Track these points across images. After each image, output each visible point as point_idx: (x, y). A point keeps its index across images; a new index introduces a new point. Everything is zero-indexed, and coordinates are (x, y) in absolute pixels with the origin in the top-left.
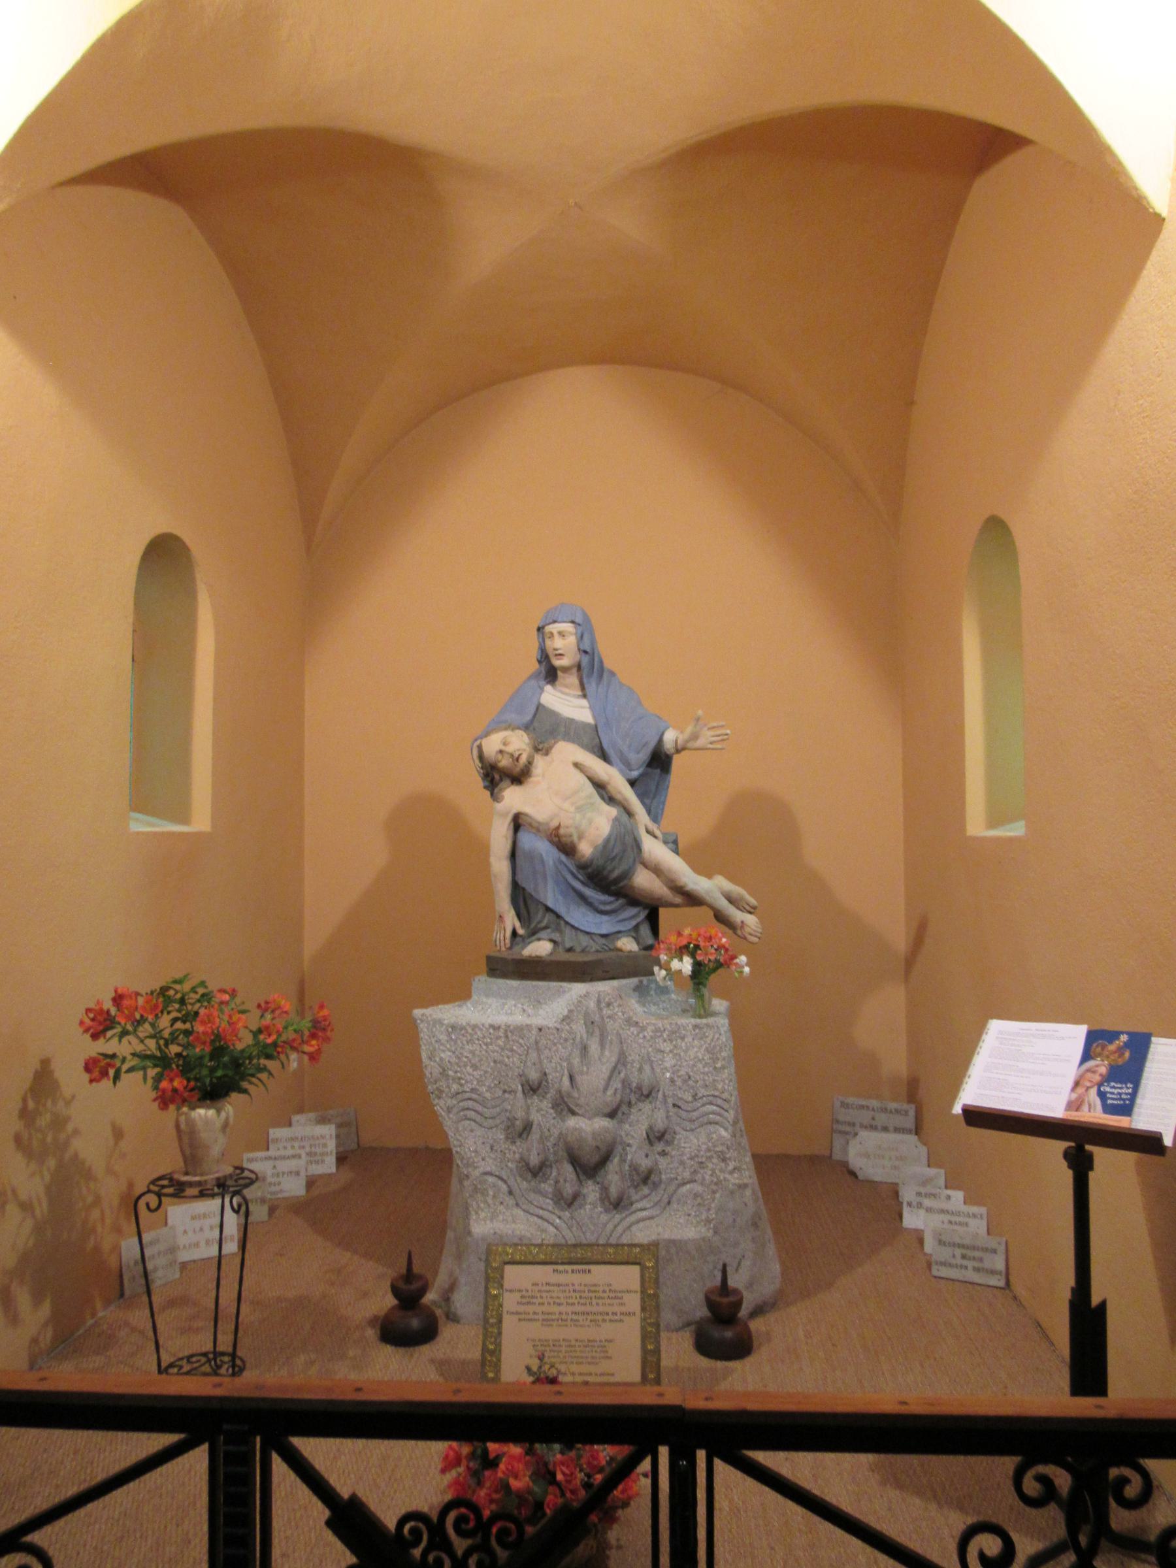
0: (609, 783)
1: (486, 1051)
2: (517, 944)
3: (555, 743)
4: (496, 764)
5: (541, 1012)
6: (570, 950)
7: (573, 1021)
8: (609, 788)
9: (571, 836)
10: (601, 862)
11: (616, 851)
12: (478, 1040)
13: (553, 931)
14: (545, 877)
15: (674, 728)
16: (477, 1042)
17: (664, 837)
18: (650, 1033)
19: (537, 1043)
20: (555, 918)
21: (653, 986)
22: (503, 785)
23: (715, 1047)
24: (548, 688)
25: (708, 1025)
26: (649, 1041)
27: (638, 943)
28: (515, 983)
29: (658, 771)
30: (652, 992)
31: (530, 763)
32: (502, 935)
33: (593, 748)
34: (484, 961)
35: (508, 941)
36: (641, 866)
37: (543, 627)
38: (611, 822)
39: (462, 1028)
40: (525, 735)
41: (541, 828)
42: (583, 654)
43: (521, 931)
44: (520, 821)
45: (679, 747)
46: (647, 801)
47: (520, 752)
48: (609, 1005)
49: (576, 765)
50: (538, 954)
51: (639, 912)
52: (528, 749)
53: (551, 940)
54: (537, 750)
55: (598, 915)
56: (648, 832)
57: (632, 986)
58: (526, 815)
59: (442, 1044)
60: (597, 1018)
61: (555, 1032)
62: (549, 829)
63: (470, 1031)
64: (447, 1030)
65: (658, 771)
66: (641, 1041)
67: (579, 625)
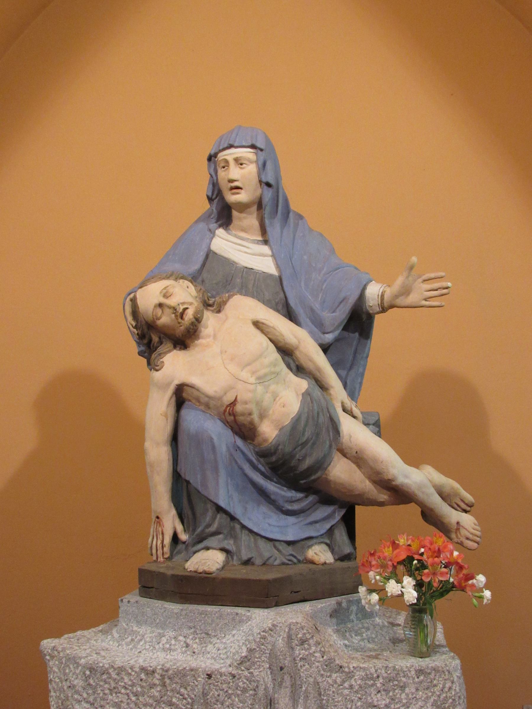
0: (297, 348)
1: (136, 704)
2: (179, 552)
3: (230, 297)
4: (154, 322)
5: (210, 647)
6: (248, 562)
7: (254, 663)
8: (297, 353)
9: (250, 414)
10: (288, 449)
11: (307, 434)
12: (126, 688)
13: (225, 538)
14: (216, 470)
15: (377, 282)
16: (123, 691)
17: (364, 417)
18: (359, 682)
19: (205, 694)
20: (229, 519)
21: (354, 608)
22: (161, 349)
23: (446, 699)
24: (221, 232)
25: (435, 669)
26: (357, 692)
27: (333, 551)
28: (174, 607)
29: (357, 335)
30: (353, 617)
31: (198, 320)
32: (159, 542)
33: (277, 304)
34: (135, 577)
35: (167, 549)
36: (340, 455)
37: (216, 155)
38: (300, 397)
39: (105, 672)
40: (192, 288)
41: (212, 403)
42: (265, 187)
43: (183, 537)
44: (184, 395)
45: (386, 305)
46: (341, 372)
47: (185, 306)
48: (303, 642)
49: (257, 324)
50: (206, 569)
51: (334, 512)
52: (196, 304)
53: (223, 550)
54: (207, 305)
55: (283, 516)
56: (345, 410)
57: (329, 611)
58: (192, 387)
59: (77, 692)
60: (287, 662)
61: (229, 679)
62: (222, 405)
63: (114, 675)
64: (84, 673)
65: (357, 335)
66: (346, 692)
67: (261, 150)
